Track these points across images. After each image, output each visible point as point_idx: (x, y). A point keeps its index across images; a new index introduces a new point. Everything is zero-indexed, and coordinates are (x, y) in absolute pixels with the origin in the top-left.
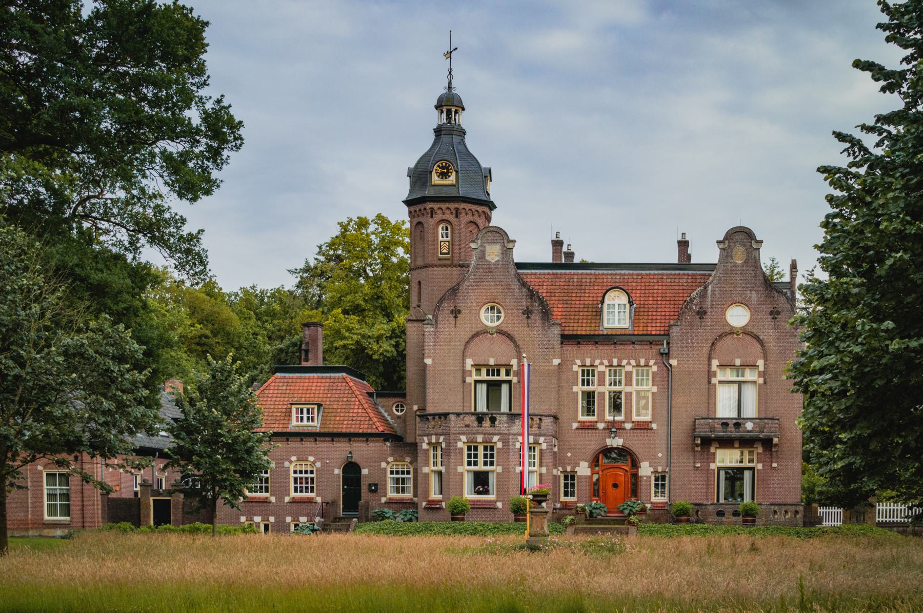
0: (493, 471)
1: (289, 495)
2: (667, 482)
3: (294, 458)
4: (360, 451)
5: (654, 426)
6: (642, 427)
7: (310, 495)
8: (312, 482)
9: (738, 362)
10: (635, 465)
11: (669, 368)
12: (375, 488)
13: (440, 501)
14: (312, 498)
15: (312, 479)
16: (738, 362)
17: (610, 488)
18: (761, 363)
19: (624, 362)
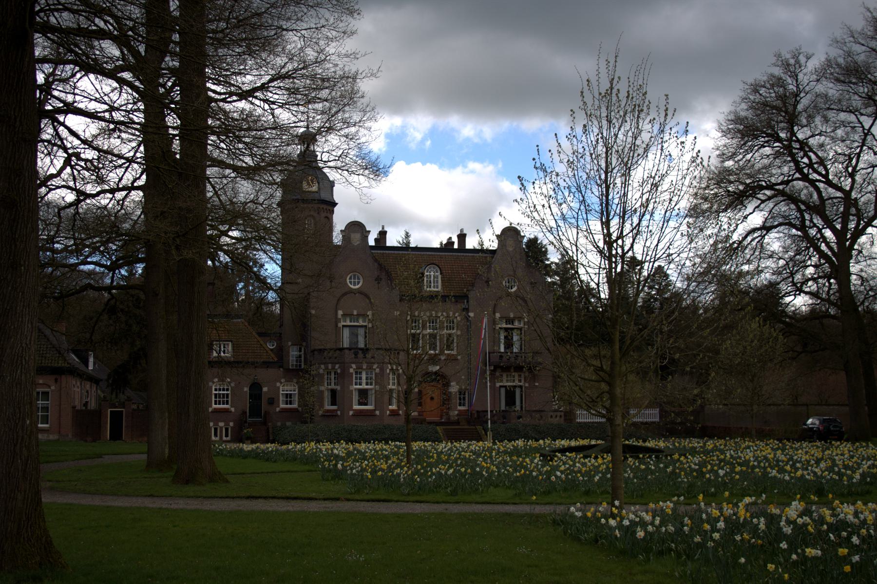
0: (371, 389)
1: (211, 406)
2: (467, 396)
3: (216, 380)
4: (262, 374)
5: (459, 357)
6: (452, 359)
7: (225, 406)
8: (227, 397)
9: (355, 313)
10: (447, 385)
11: (467, 318)
12: (272, 401)
13: (336, 410)
14: (228, 409)
15: (227, 395)
16: (355, 313)
17: (428, 400)
18: (369, 313)
19: (440, 314)
